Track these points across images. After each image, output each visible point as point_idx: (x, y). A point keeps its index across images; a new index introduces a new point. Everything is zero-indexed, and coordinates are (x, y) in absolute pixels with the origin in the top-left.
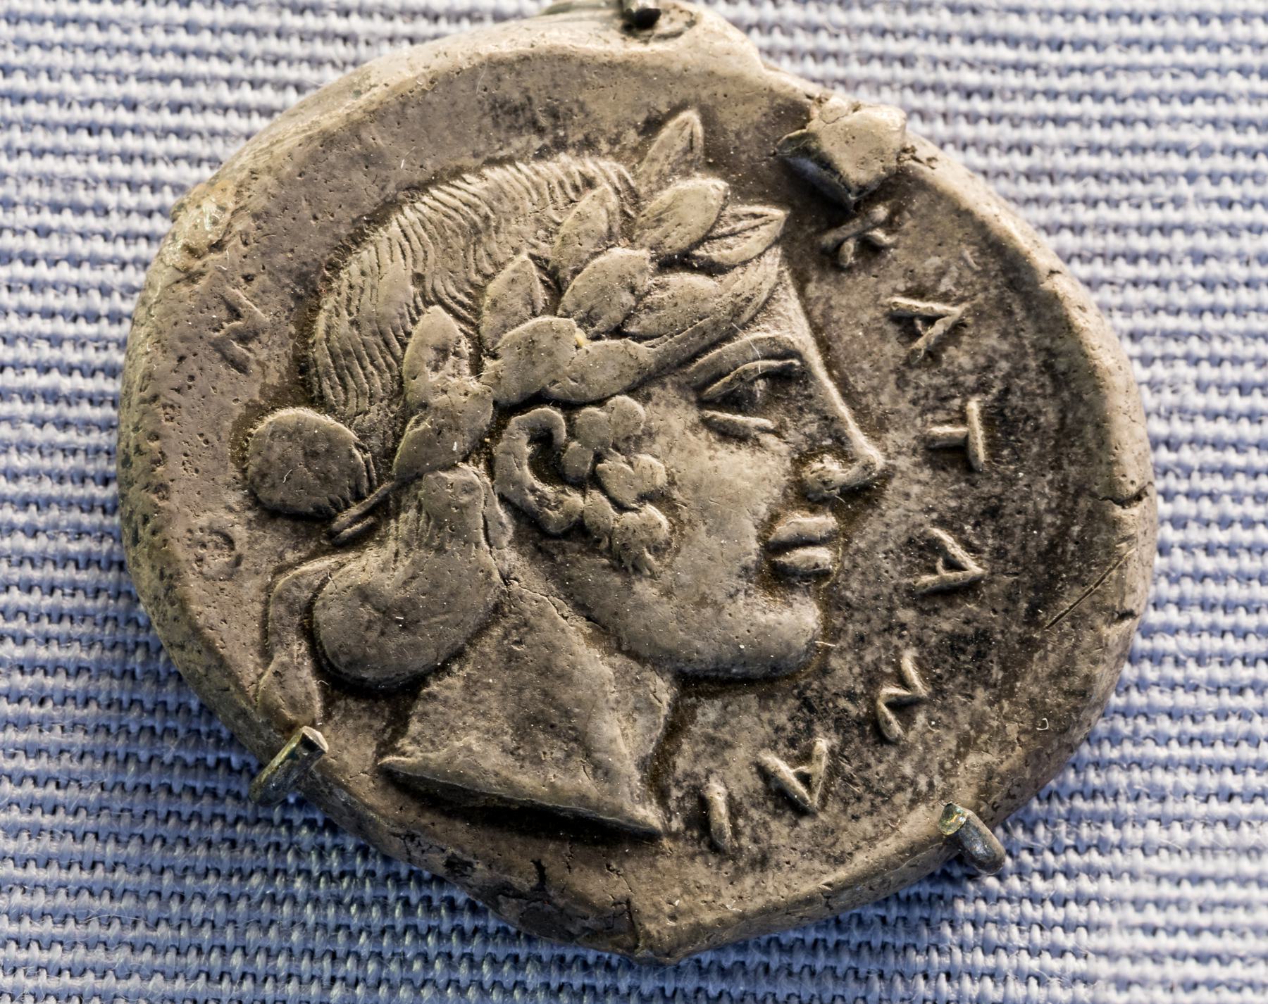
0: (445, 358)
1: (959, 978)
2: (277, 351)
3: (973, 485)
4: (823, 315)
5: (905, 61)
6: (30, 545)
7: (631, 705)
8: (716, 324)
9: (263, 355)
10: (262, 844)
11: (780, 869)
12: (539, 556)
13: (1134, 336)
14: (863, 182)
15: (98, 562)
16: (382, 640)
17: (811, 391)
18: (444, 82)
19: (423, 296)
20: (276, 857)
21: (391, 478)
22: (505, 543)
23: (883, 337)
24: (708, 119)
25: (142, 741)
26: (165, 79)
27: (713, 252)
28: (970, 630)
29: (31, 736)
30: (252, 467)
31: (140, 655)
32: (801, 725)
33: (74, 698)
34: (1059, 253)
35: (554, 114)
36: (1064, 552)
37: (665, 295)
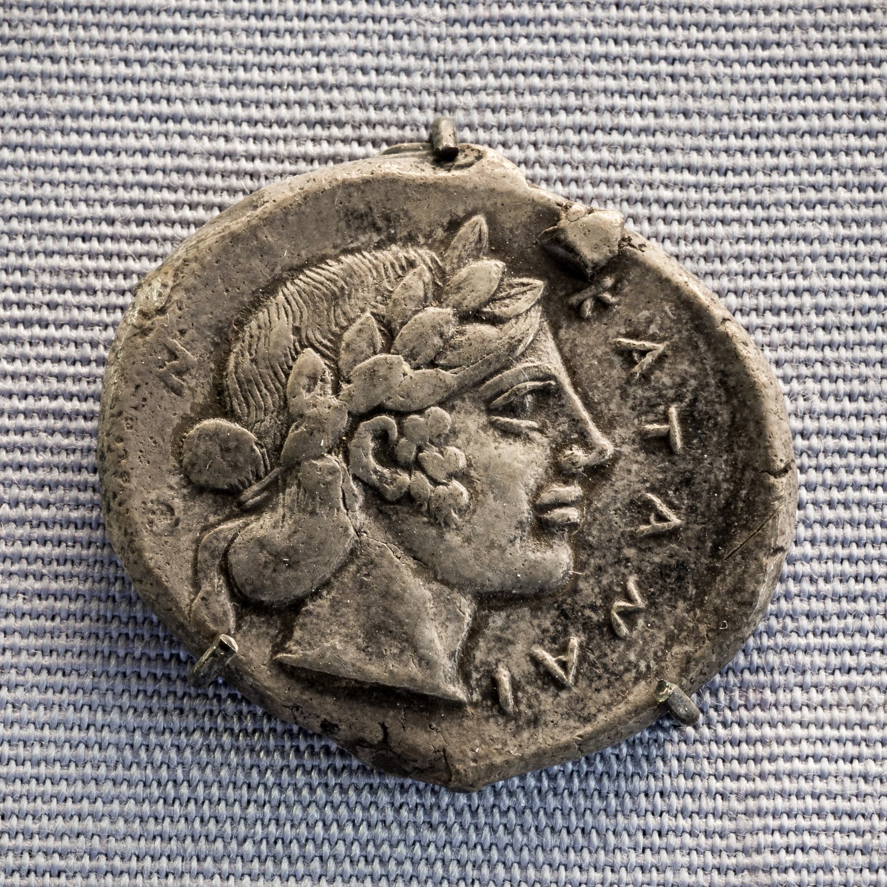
0: (315, 383)
1: (669, 796)
2: (202, 381)
3: (674, 464)
4: (571, 351)
5: (622, 184)
6: (45, 514)
7: (444, 616)
8: (498, 357)
9: (193, 383)
10: (201, 711)
11: (547, 726)
12: (381, 516)
13: (778, 363)
14: (596, 260)
15: (90, 524)
16: (274, 575)
17: (563, 402)
18: (311, 198)
19: (300, 342)
20: (210, 720)
21: (279, 465)
22: (357, 508)
23: (611, 365)
24: (491, 221)
25: (120, 643)
26: (133, 204)
27: (497, 309)
28: (673, 562)
29: (46, 641)
30: (186, 458)
31: (118, 586)
32: (560, 628)
33: (75, 615)
34: (729, 308)
35: (387, 219)
36: (736, 508)
37: (463, 338)
